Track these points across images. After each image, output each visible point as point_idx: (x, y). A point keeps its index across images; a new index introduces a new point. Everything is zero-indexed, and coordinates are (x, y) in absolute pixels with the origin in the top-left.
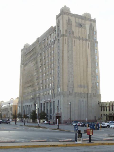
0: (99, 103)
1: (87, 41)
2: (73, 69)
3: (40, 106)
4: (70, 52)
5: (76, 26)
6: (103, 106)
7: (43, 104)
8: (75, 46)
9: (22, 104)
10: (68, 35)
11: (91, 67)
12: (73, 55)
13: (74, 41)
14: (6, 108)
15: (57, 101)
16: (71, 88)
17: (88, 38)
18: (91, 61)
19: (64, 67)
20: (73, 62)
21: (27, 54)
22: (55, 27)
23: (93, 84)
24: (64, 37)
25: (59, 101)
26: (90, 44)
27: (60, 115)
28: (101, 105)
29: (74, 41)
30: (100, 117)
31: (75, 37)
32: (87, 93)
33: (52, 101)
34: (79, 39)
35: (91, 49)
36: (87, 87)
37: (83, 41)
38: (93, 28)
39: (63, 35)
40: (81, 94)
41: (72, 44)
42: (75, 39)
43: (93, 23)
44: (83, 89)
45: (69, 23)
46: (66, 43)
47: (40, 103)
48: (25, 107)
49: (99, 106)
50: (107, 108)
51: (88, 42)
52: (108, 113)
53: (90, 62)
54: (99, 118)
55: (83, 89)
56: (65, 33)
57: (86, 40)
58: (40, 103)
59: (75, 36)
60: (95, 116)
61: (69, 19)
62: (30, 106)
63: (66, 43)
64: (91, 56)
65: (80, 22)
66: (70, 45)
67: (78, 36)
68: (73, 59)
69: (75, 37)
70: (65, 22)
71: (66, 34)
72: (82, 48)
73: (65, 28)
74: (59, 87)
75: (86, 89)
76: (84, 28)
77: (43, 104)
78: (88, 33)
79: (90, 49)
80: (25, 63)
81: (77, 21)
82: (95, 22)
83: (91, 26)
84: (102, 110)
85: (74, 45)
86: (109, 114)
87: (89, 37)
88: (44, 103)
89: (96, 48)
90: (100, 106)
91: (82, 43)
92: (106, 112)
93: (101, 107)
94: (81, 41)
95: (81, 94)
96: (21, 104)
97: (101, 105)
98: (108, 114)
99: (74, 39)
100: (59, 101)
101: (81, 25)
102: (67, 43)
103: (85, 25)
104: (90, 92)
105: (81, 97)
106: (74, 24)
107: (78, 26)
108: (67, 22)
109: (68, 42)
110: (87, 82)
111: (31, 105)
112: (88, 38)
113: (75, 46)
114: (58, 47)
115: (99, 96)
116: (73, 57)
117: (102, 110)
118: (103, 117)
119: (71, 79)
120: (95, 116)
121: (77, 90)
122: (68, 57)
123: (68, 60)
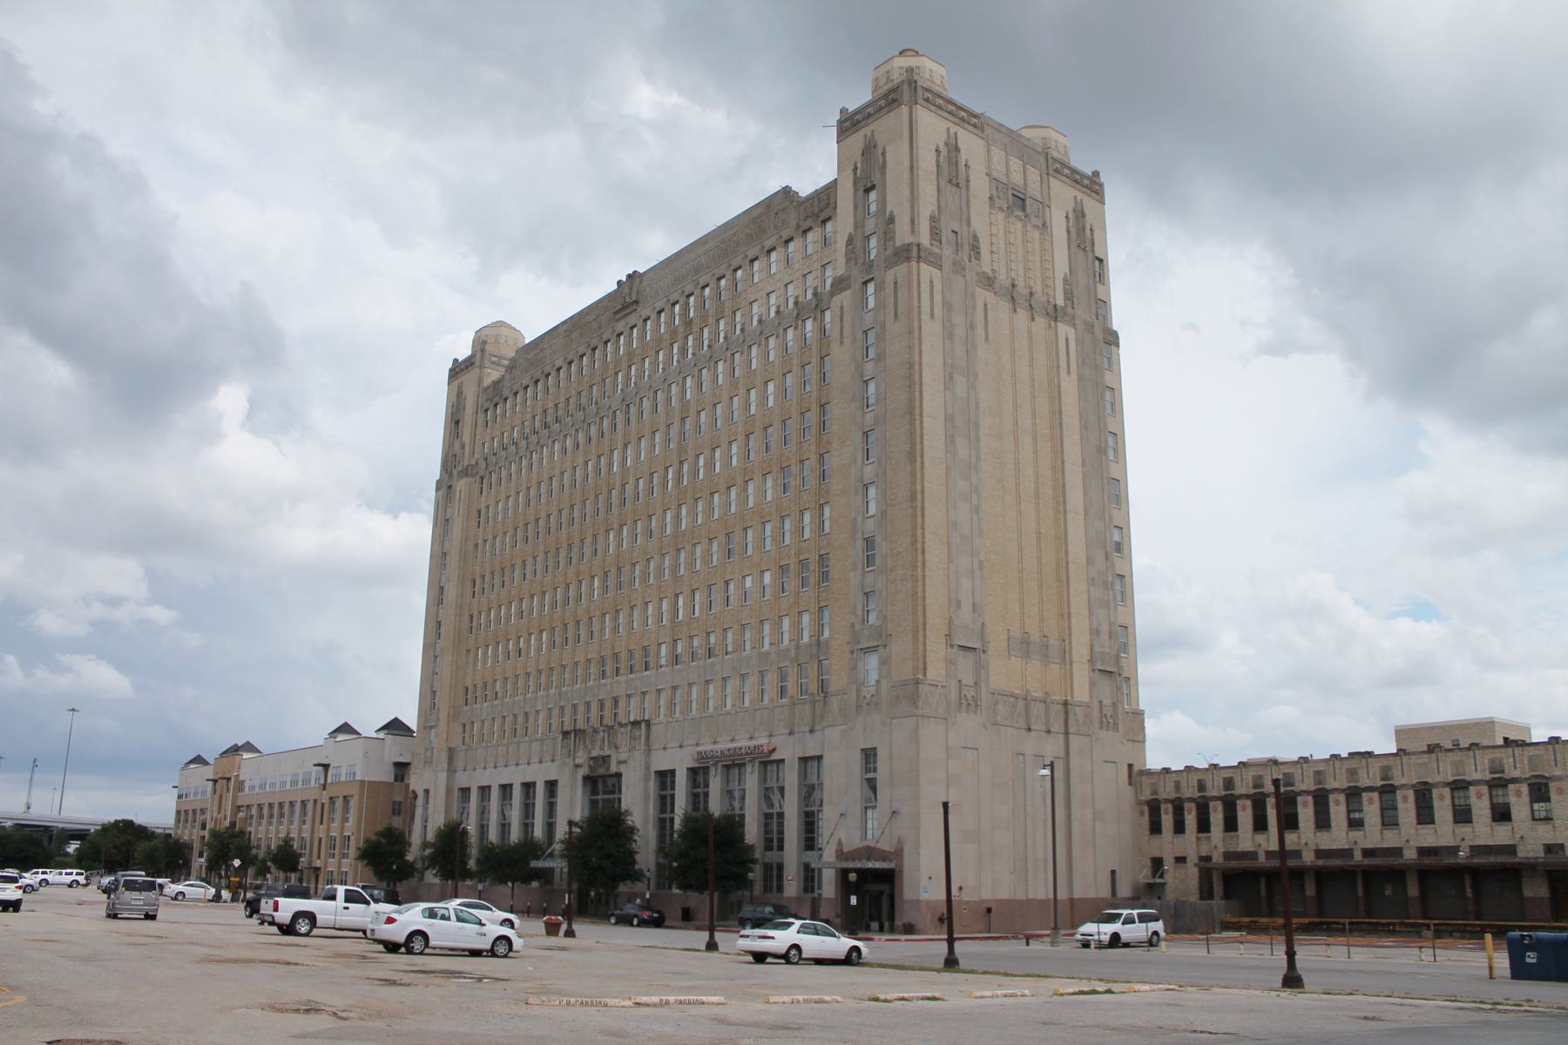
0: (1136, 775)
1: (1056, 320)
2: (977, 509)
3: (646, 789)
4: (960, 381)
5: (991, 198)
6: (1173, 796)
7: (681, 780)
8: (987, 339)
9: (451, 770)
10: (947, 252)
11: (1081, 508)
12: (977, 407)
13: (842, 342)
14: (265, 801)
15: (857, 760)
16: (970, 654)
17: (1060, 302)
18: (1083, 465)
19: (923, 492)
20: (978, 458)
21: (506, 392)
22: (833, 186)
23: (1095, 632)
24: (923, 266)
25: (869, 755)
26: (1077, 341)
27: (891, 865)
28: (1155, 792)
29: (842, 342)
30: (1145, 876)
31: (988, 281)
32: (1066, 704)
33: (788, 751)
34: (1011, 294)
35: (1080, 378)
36: (1065, 656)
37: (1033, 319)
38: (962, 168)
39: (915, 253)
40: (1027, 708)
41: (972, 327)
42: (989, 295)
43: (1089, 204)
44: (1035, 665)
45: (952, 173)
46: (932, 316)
47: (648, 767)
48: (528, 809)
49: (1140, 803)
50: (1208, 813)
51: (1064, 329)
52: (1221, 849)
53: (1079, 470)
54: (1136, 889)
55: (1035, 665)
56: (925, 238)
57: (1055, 314)
58: (648, 767)
59: (988, 270)
60: (1113, 872)
61: (954, 148)
62: (540, 790)
63: (932, 316)
64: (1084, 427)
65: (1017, 178)
66: (960, 332)
67: (1002, 278)
68: (978, 440)
69: (988, 281)
70: (927, 161)
71: (936, 250)
72: (1031, 366)
73: (927, 207)
74: (873, 649)
75: (1055, 669)
76: (1040, 223)
77: (681, 780)
78: (1061, 265)
79: (1074, 375)
80: (482, 464)
81: (999, 170)
82: (1096, 192)
83: (1077, 218)
84: (1155, 828)
85: (980, 331)
86: (1228, 855)
87: (1069, 296)
88: (698, 775)
89: (1108, 378)
90: (1147, 795)
91: (1030, 332)
92: (1198, 839)
93: (1154, 808)
94: (1022, 314)
95: (1027, 708)
96: (443, 776)
97: (1155, 792)
98: (1217, 858)
99: (982, 295)
100: (869, 755)
101: (1020, 201)
102: (938, 311)
103: (1044, 204)
104: (1081, 693)
105: (1029, 730)
106: (980, 185)
107: (1005, 206)
108: (938, 162)
109: (947, 306)
110: (1065, 616)
111: (552, 786)
112: (1060, 302)
113: (987, 339)
114: (860, 336)
115: (1133, 725)
116: (977, 425)
117: (1155, 828)
118: (1168, 878)
119: (966, 584)
120: (1113, 872)
121: (1004, 673)
122: (949, 419)
123: (950, 440)
